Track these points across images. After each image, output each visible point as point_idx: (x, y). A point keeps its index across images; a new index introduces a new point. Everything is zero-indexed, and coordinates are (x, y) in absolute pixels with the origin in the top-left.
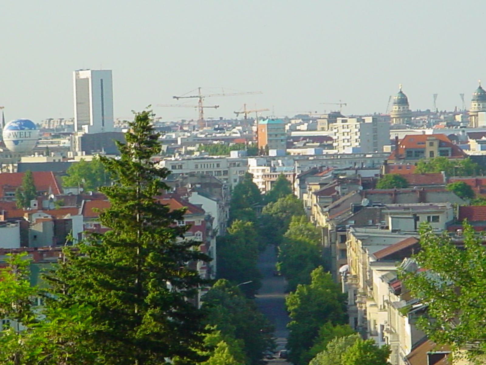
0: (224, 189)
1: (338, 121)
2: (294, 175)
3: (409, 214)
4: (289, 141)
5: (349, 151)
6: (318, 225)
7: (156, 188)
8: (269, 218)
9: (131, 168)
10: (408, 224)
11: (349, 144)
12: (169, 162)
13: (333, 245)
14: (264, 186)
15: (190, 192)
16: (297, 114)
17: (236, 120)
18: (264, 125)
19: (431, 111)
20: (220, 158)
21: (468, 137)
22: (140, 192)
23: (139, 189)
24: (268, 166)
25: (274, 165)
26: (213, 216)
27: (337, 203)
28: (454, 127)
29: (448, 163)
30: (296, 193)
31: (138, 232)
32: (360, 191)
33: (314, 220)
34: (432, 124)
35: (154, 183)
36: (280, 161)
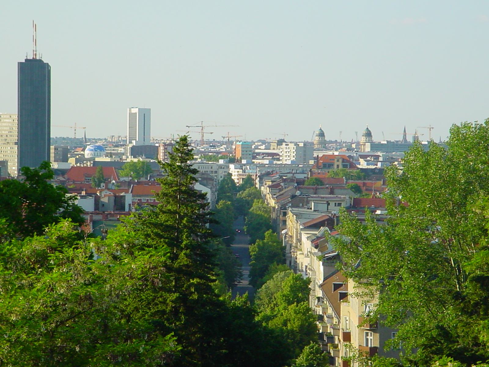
2: (256, 175)
3: (324, 201)
5: (289, 162)
6: (269, 205)
11: (289, 158)
14: (238, 181)
27: (281, 193)
33: (267, 202)
36: (248, 167)
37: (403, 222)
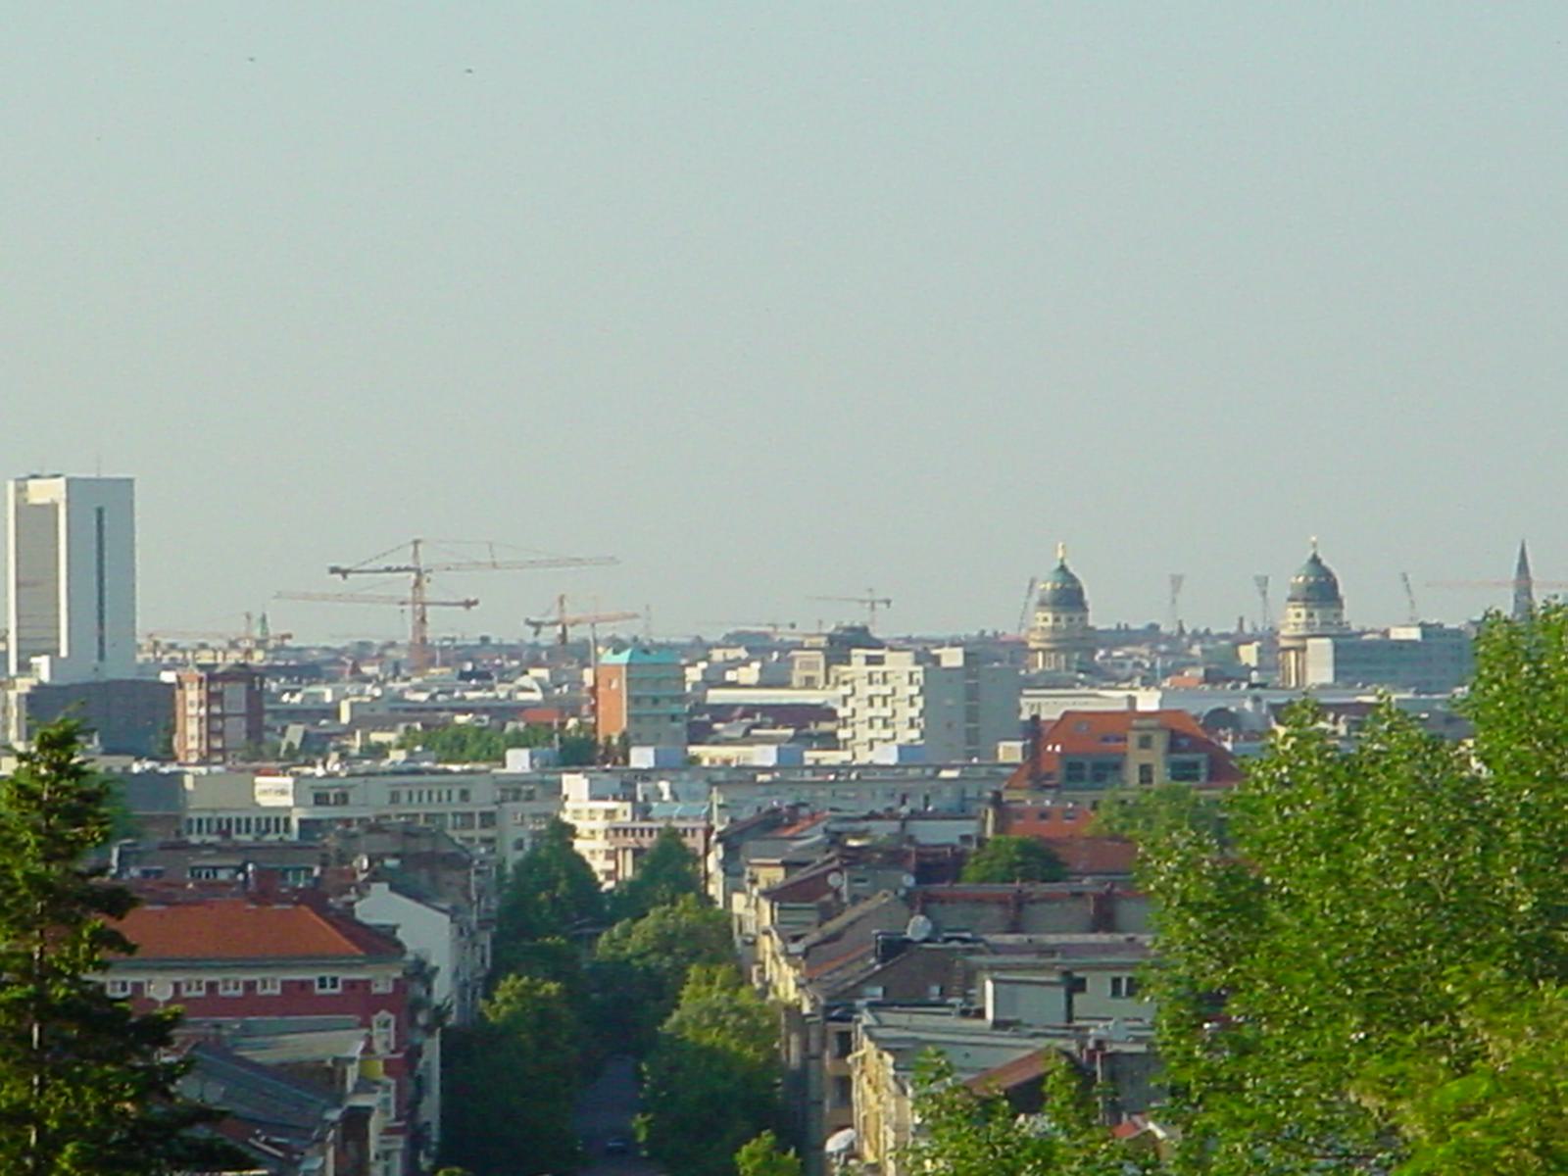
0: (478, 872)
1: (854, 660)
2: (709, 831)
3: (1049, 968)
4: (696, 718)
5: (888, 756)
6: (771, 997)
7: (92, 951)
8: (619, 968)
9: (16, 889)
10: (1045, 1003)
11: (888, 734)
12: (309, 782)
13: (813, 1063)
14: (611, 865)
15: (365, 880)
16: (731, 630)
17: (535, 646)
18: (618, 666)
19: (1163, 629)
20: (471, 772)
21: (1272, 719)
22: (45, 959)
23: (42, 952)
24: (624, 800)
25: (646, 797)
26: (434, 963)
27: (832, 926)
28: (1229, 686)
29: (1196, 805)
30: (712, 890)
31: (36, 1081)
32: (908, 889)
33: (761, 979)
34: (1159, 674)
35: (85, 934)
36: (664, 786)
37: (1239, 1120)
